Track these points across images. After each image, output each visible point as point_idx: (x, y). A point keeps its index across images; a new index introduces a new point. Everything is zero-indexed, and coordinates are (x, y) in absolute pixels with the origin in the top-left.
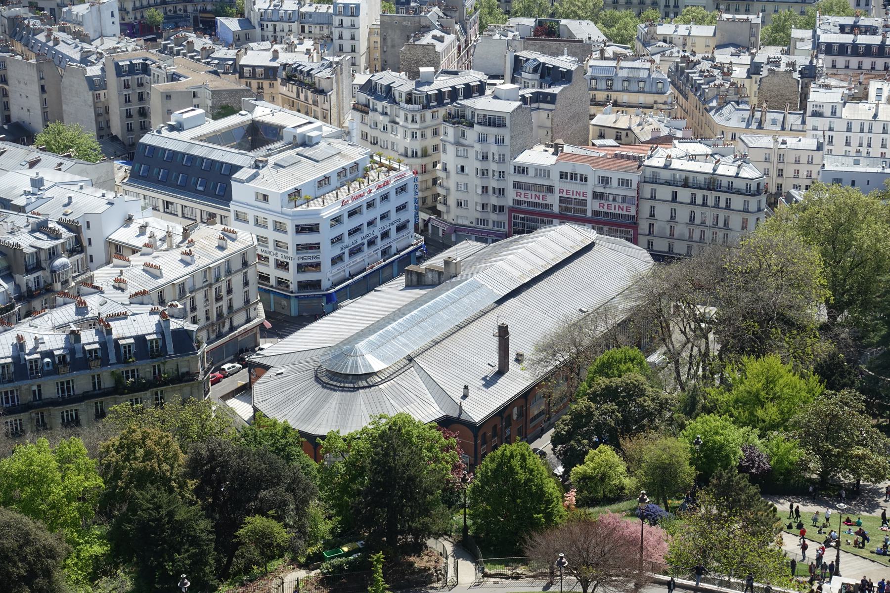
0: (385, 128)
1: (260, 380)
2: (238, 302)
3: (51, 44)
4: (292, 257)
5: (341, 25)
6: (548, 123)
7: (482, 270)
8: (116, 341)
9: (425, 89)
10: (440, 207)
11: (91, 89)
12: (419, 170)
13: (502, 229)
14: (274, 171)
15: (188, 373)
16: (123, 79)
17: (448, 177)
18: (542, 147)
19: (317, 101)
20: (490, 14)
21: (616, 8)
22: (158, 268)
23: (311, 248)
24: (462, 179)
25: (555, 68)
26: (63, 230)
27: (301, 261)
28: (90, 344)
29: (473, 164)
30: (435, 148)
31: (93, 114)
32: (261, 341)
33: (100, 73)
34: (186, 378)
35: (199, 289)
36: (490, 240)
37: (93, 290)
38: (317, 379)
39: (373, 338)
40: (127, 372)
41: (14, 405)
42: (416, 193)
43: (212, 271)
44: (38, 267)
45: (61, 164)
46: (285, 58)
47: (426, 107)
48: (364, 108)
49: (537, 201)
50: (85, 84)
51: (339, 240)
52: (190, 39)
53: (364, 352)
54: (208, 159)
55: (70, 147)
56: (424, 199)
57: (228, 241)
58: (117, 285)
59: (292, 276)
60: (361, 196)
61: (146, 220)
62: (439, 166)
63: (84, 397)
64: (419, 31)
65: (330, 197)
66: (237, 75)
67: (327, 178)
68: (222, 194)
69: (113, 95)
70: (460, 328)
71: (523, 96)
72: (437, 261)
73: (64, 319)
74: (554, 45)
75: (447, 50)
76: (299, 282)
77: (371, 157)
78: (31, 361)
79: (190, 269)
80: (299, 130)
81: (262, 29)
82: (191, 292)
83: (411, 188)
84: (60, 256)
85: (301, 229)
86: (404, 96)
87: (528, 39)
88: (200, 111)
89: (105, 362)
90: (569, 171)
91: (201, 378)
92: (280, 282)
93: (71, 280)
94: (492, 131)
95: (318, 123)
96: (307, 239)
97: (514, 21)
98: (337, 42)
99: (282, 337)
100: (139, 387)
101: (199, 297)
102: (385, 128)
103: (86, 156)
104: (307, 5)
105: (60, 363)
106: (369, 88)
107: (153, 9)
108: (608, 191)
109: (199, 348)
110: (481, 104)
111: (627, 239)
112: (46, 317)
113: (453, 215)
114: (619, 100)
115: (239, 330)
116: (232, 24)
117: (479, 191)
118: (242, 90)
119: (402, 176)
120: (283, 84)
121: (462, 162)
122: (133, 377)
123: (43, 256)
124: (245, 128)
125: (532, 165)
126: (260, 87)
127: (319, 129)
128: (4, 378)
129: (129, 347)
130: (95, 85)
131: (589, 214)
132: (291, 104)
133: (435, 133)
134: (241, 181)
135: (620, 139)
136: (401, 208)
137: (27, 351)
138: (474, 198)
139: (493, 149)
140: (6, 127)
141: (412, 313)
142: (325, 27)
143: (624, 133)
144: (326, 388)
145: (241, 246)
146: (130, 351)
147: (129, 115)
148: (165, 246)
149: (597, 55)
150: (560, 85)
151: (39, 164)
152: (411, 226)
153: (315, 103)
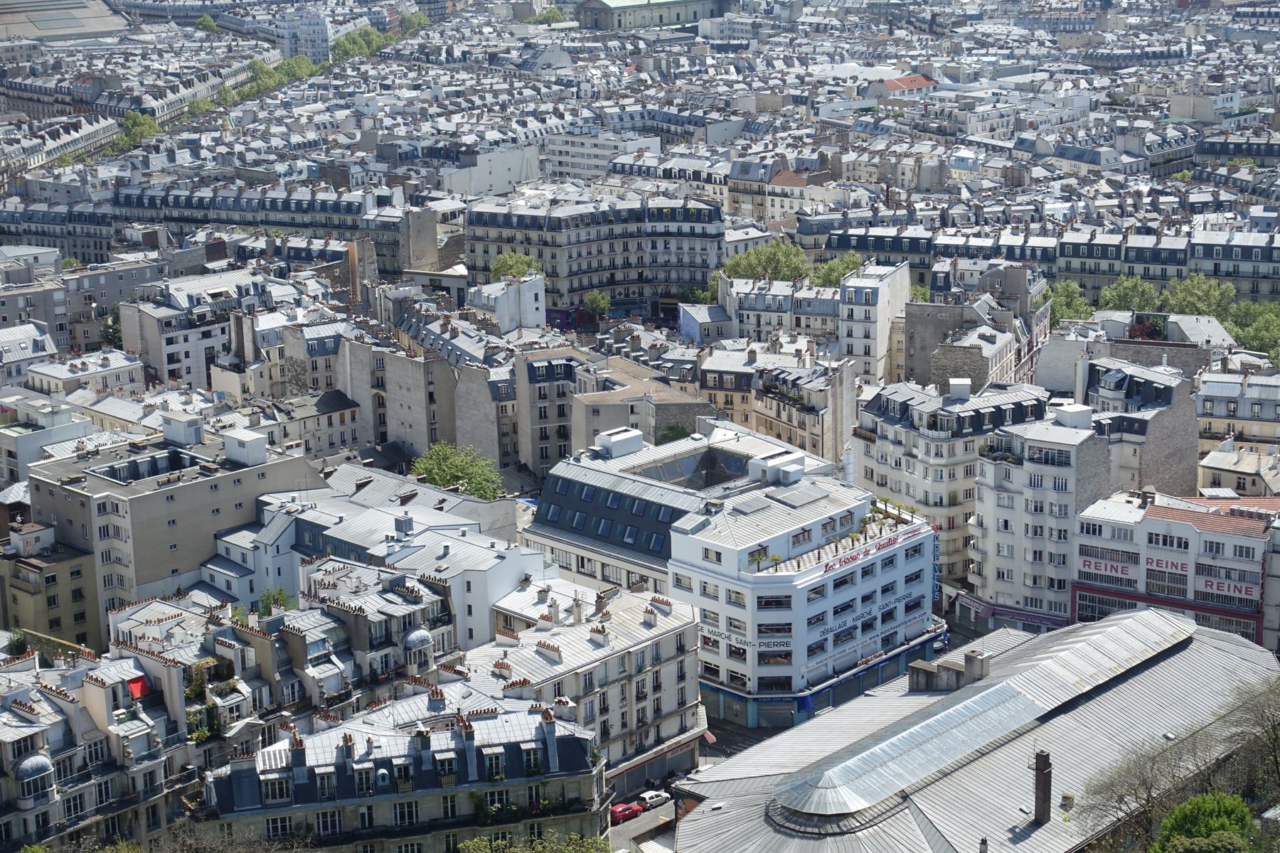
0: (898, 464)
1: (689, 817)
2: (669, 704)
3: (447, 336)
4: (752, 642)
5: (851, 316)
6: (1135, 462)
7: (1020, 671)
8: (479, 749)
9: (957, 408)
10: (972, 579)
11: (495, 399)
12: (945, 525)
13: (1062, 614)
14: (731, 519)
15: (577, 800)
16: (538, 385)
17: (984, 536)
18: (1125, 497)
19: (804, 423)
20: (1068, 305)
21: (1254, 300)
22: (557, 650)
23: (778, 631)
24: (1005, 539)
25: (1148, 383)
26: (424, 591)
27: (763, 649)
28: (442, 751)
29: (1021, 519)
30: (969, 494)
31: (496, 434)
32: (701, 760)
33: (507, 377)
34: (574, 807)
35: (614, 682)
36: (1044, 628)
37: (456, 676)
38: (768, 818)
39: (851, 762)
40: (492, 794)
41: (334, 833)
42: (936, 558)
43: (633, 657)
44: (387, 641)
45: (443, 501)
46: (766, 361)
47: (957, 434)
48: (869, 434)
49: (1114, 574)
50: (487, 393)
51: (818, 620)
52: (635, 333)
53: (836, 782)
54: (641, 500)
55: (458, 478)
56: (951, 567)
57: (659, 615)
58: (497, 671)
59: (750, 670)
60: (854, 558)
61: (549, 582)
62: (972, 520)
63: (433, 826)
64: (961, 328)
65: (809, 560)
66: (697, 384)
67: (805, 532)
68: (658, 548)
69: (523, 408)
70: (982, 754)
71: (1098, 422)
72: (956, 657)
73: (411, 715)
74: (1154, 350)
75: (1000, 354)
76: (760, 679)
77: (874, 503)
78: (360, 772)
79: (601, 653)
80: (771, 463)
81: (741, 321)
82: (601, 686)
83: (928, 550)
84: (418, 627)
85: (766, 603)
86: (925, 418)
87: (1117, 342)
88: (636, 433)
89: (462, 778)
90: (1162, 532)
91: (595, 808)
92: (734, 678)
93: (431, 661)
94: (1050, 471)
95: (799, 453)
96: (774, 617)
97: (1100, 316)
98: (845, 341)
99: (729, 755)
100: (507, 816)
101: (613, 693)
102: (898, 464)
103: (481, 492)
104: (805, 288)
105: (400, 777)
106: (878, 406)
107: (596, 291)
108: (1218, 563)
109: (594, 765)
110: (1035, 432)
111: (1245, 635)
112: (386, 711)
113: (991, 591)
114: (1246, 432)
115: (668, 743)
116: (699, 314)
117: (1030, 557)
118: (698, 405)
119: (915, 532)
120: (759, 397)
121: (1005, 514)
122: (500, 801)
123: (394, 627)
124: (698, 458)
125: (1108, 523)
126: (729, 402)
127: (800, 461)
128: (323, 794)
129: (497, 758)
130: (500, 393)
131: (1190, 596)
132: (769, 427)
133: (969, 472)
134: (684, 532)
135: (1244, 489)
136: (913, 578)
137: (356, 758)
138: (1022, 567)
139: (1051, 497)
140: (379, 448)
141: (912, 730)
142: (829, 319)
143: (1249, 479)
144: (779, 832)
145: (676, 624)
146: (497, 764)
147: (544, 436)
148: (571, 620)
149: (1217, 366)
150: (1154, 408)
151: (415, 500)
152: (928, 604)
153: (802, 425)
